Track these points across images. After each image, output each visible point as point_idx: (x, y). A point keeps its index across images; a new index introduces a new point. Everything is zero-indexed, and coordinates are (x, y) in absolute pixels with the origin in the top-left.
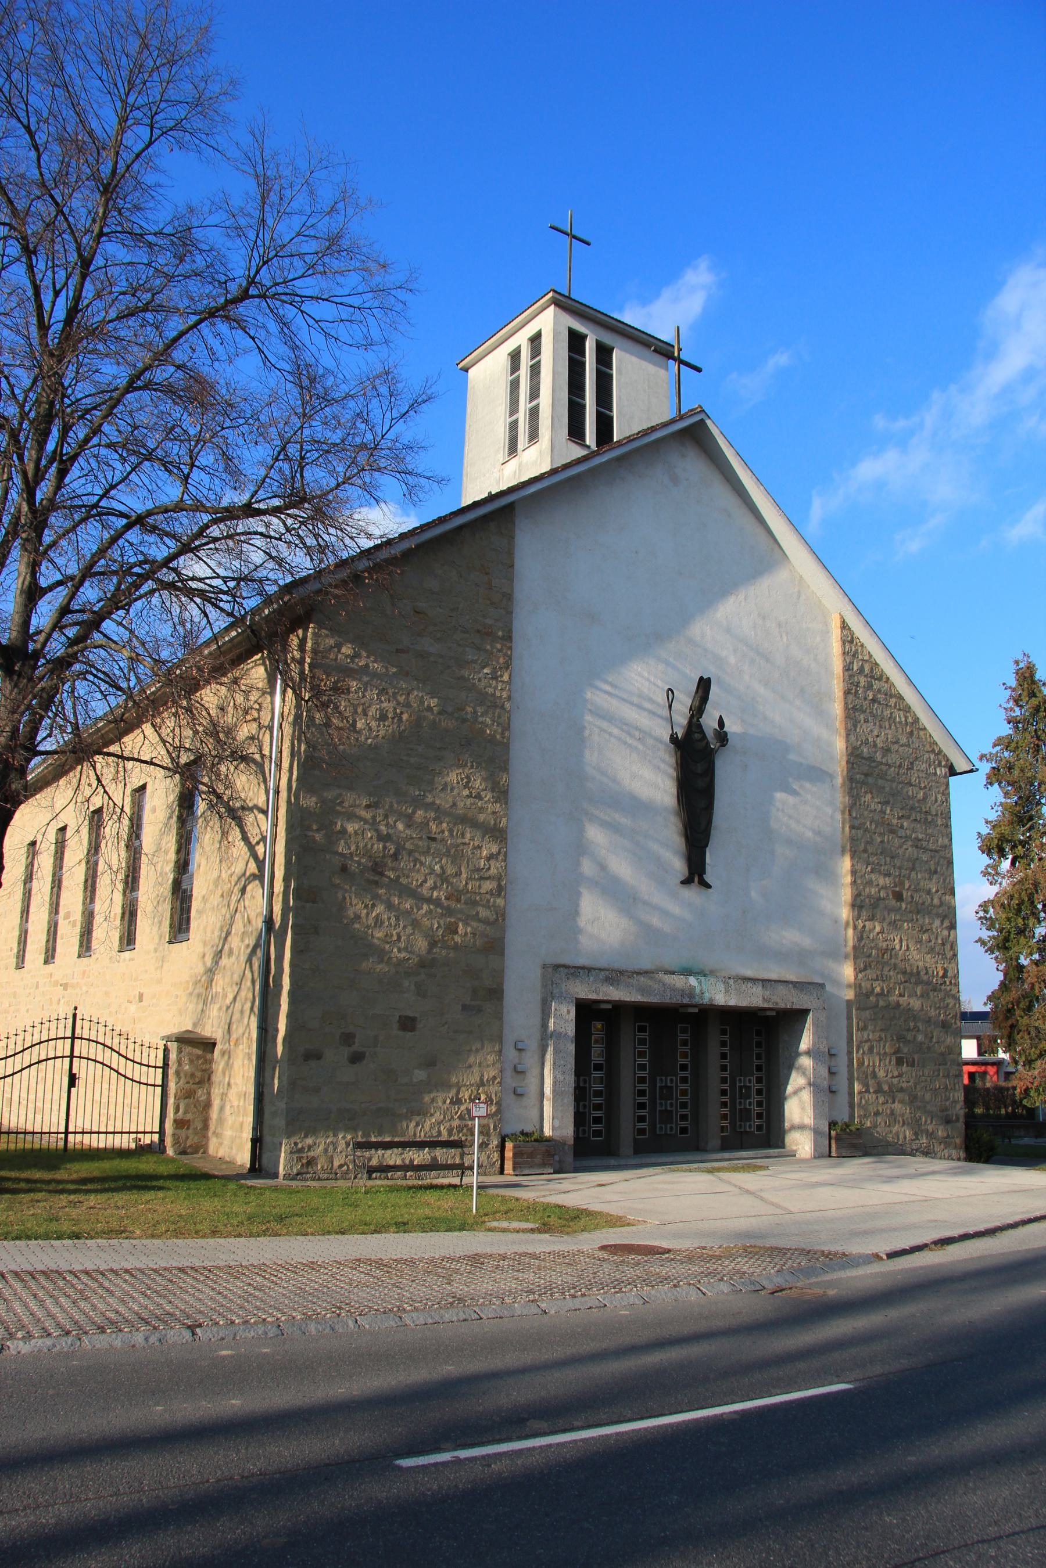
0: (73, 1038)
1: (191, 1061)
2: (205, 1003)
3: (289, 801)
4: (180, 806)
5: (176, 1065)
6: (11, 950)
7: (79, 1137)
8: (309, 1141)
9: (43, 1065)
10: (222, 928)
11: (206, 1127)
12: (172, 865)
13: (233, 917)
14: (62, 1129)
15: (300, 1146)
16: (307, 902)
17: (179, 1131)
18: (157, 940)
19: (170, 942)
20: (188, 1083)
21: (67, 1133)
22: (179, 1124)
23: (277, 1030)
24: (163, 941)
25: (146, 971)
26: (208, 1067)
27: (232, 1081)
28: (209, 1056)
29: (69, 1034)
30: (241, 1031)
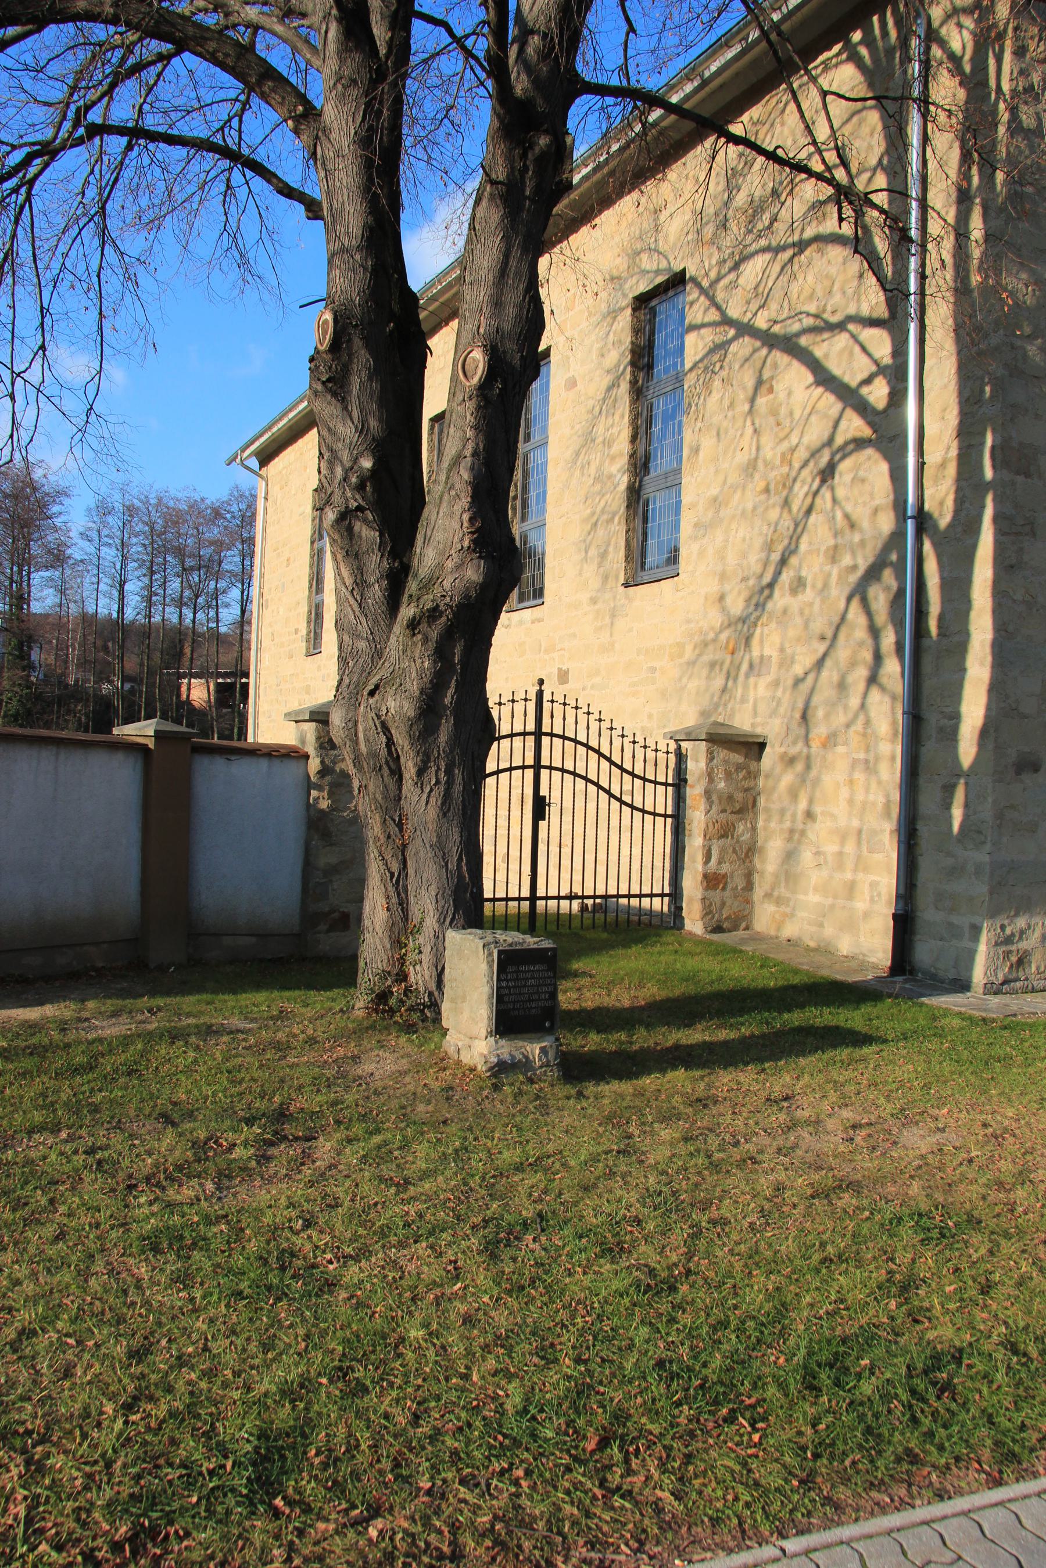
0: (538, 734)
1: (728, 775)
2: (731, 675)
3: (962, 290)
4: (633, 364)
5: (704, 782)
6: (296, 631)
7: (552, 903)
8: (1021, 922)
9: (504, 777)
10: (769, 547)
11: (749, 886)
12: (623, 461)
13: (799, 528)
14: (526, 893)
15: (1008, 931)
16: (1018, 473)
17: (711, 894)
18: (595, 583)
19: (626, 585)
20: (724, 811)
21: (533, 898)
22: (712, 881)
23: (955, 717)
24: (611, 583)
25: (574, 635)
26: (752, 784)
27: (818, 809)
28: (753, 765)
29: (531, 727)
30: (840, 719)
